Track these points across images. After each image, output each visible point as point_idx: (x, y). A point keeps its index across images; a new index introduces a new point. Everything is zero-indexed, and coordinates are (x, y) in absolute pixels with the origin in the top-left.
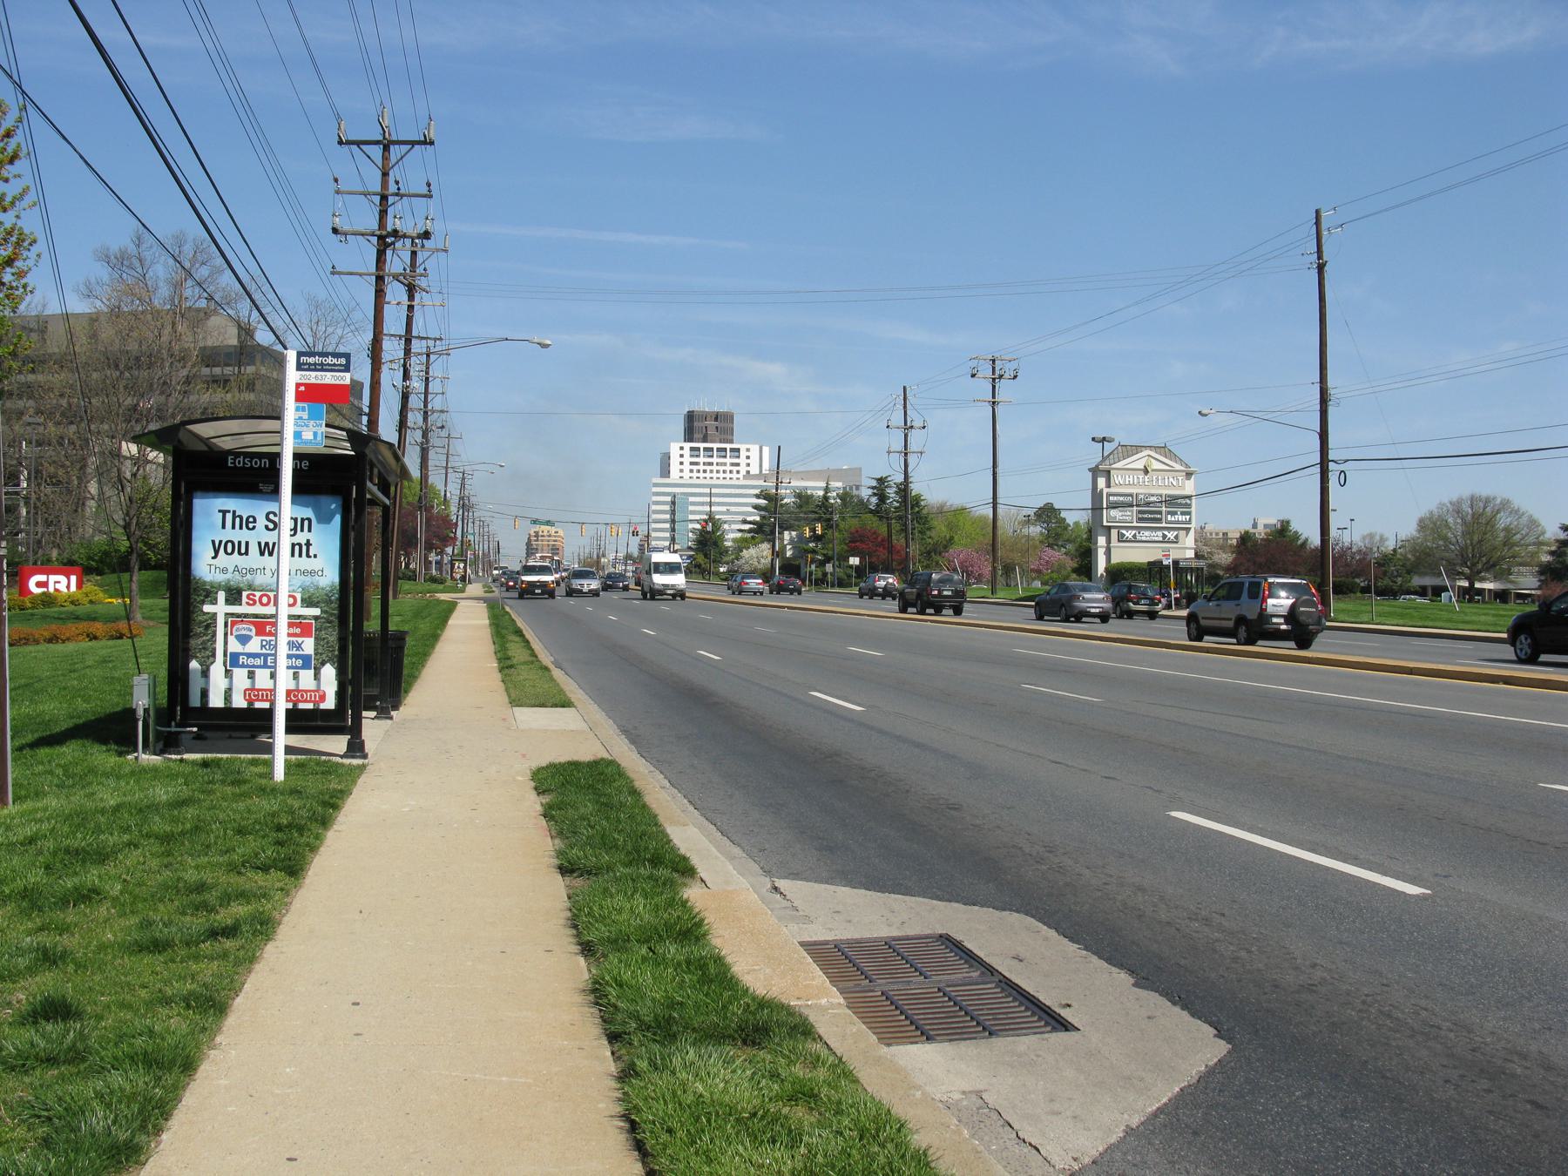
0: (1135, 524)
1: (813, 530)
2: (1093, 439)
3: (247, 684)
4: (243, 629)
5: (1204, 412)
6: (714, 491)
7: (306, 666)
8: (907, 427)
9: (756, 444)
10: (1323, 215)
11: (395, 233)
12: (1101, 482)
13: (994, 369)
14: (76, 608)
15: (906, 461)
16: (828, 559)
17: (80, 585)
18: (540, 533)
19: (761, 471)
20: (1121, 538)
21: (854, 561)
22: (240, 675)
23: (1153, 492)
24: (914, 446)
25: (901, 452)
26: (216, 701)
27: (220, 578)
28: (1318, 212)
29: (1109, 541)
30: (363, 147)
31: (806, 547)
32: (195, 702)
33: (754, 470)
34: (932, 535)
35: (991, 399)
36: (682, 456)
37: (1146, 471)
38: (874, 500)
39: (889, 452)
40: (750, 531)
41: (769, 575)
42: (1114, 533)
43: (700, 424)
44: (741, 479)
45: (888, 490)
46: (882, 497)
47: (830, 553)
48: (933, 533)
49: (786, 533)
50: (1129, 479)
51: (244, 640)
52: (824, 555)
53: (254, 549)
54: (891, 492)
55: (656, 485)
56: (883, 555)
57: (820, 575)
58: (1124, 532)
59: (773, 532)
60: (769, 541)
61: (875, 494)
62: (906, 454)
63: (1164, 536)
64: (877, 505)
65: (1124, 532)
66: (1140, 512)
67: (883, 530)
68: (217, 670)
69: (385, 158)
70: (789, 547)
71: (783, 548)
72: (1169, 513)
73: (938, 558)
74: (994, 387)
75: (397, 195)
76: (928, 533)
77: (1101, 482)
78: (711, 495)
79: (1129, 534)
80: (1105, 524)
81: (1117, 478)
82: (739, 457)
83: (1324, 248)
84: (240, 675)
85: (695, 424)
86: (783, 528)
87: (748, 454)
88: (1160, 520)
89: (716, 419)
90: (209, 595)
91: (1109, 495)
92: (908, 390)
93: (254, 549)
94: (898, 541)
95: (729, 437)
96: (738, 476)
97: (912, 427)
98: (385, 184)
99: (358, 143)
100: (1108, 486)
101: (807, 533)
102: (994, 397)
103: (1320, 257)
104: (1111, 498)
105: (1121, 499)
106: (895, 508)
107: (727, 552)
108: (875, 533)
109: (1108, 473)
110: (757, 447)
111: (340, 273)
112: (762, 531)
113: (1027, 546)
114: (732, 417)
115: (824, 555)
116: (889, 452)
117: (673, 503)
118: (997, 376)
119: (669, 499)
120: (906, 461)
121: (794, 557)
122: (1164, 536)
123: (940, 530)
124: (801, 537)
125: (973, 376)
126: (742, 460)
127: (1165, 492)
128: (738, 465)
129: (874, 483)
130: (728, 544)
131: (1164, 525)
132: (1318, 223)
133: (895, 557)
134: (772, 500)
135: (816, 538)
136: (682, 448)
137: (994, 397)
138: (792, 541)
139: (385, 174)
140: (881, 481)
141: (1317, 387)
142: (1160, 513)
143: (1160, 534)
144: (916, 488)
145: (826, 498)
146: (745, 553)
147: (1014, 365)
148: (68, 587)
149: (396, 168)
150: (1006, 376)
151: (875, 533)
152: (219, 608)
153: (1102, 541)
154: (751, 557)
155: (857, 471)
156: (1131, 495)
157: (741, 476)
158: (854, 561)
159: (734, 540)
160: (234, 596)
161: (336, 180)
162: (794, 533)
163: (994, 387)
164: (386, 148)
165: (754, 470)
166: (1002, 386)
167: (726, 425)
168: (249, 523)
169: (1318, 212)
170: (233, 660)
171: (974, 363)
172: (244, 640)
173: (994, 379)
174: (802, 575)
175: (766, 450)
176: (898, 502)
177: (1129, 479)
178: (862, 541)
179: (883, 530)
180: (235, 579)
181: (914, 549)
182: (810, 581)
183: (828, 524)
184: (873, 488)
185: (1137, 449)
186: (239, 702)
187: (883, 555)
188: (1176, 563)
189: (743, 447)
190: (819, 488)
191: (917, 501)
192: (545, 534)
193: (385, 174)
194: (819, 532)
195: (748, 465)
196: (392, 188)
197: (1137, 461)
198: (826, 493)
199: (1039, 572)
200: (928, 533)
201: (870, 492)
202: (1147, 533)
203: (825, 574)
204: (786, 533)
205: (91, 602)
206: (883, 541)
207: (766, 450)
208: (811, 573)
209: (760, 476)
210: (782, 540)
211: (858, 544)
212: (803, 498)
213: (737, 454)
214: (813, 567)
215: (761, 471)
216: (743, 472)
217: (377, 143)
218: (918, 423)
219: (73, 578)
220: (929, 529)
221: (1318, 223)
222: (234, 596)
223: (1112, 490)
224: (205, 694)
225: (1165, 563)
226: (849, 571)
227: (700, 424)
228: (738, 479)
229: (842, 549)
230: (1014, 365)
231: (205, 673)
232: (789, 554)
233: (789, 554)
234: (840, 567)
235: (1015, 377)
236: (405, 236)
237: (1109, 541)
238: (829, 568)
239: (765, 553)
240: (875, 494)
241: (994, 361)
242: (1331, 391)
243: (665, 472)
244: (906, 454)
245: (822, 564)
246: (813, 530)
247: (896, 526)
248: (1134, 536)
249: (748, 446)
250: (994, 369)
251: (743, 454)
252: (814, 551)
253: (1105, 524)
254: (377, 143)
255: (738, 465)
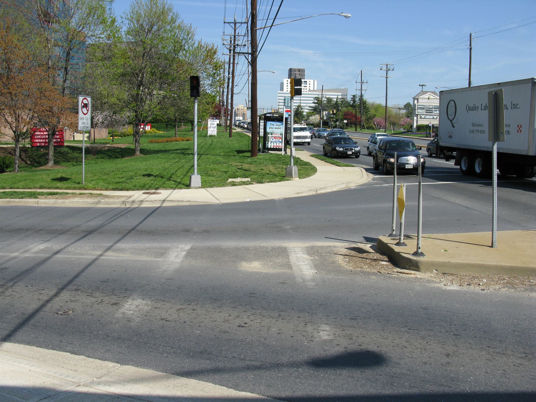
0: (425, 114)
1: (333, 111)
2: (419, 85)
3: (273, 145)
4: (273, 138)
5: (437, 87)
6: (301, 98)
7: (280, 143)
8: (362, 83)
9: (312, 79)
10: (472, 35)
11: (238, 45)
12: (416, 102)
13: (387, 68)
14: (151, 134)
15: (361, 92)
16: (337, 121)
17: (151, 128)
18: (239, 109)
19: (314, 89)
20: (421, 118)
21: (345, 121)
22: (272, 144)
23: (430, 105)
24: (364, 88)
25: (360, 90)
26: (269, 147)
27: (270, 132)
28: (471, 34)
29: (417, 118)
30: (230, 24)
31: (330, 116)
32: (267, 147)
33: (312, 89)
34: (370, 113)
35: (386, 76)
36: (287, 86)
37: (429, 99)
38: (352, 102)
39: (356, 90)
40: (312, 110)
41: (319, 125)
42: (419, 116)
43: (294, 73)
44: (307, 91)
45: (356, 99)
46: (354, 102)
47: (338, 119)
48: (370, 113)
49: (324, 112)
50: (424, 101)
51: (273, 139)
52: (336, 119)
53: (274, 128)
54: (357, 99)
55: (279, 93)
56: (354, 119)
57: (335, 125)
58: (422, 116)
59: (320, 112)
60: (318, 114)
61: (352, 100)
62: (361, 91)
63: (433, 117)
64: (353, 104)
65: (422, 116)
66: (426, 110)
67: (354, 112)
68: (269, 143)
69: (235, 27)
70: (325, 116)
71: (323, 116)
72: (435, 111)
73: (371, 121)
74: (387, 73)
75: (238, 35)
76: (368, 113)
77: (416, 102)
78: (300, 100)
79: (423, 117)
80: (416, 113)
81: (420, 101)
82: (306, 84)
83: (472, 44)
84: (272, 144)
85: (292, 73)
86: (324, 110)
87: (310, 83)
88: (432, 113)
89: (299, 71)
90: (269, 134)
91: (418, 105)
92: (362, 71)
93: (274, 128)
94: (358, 115)
95: (304, 77)
96: (306, 90)
97: (363, 82)
98: (235, 33)
99: (229, 23)
100: (418, 102)
101: (331, 112)
102: (387, 76)
103: (470, 46)
104: (418, 106)
105: (421, 106)
106: (358, 105)
107: (304, 117)
108: (352, 113)
109: (418, 99)
110: (313, 81)
111: (224, 54)
112: (316, 110)
113: (398, 116)
114: (304, 70)
115: (336, 119)
116: (356, 90)
117: (285, 100)
118: (388, 69)
119: (283, 98)
120: (361, 92)
121: (327, 119)
122: (433, 117)
123: (372, 112)
124: (329, 113)
125: (381, 69)
126: (308, 85)
127: (434, 105)
128: (306, 87)
129: (352, 97)
130: (305, 114)
131: (433, 114)
132: (470, 37)
133: (358, 120)
134: (318, 101)
135: (333, 114)
136: (287, 81)
137: (387, 76)
138: (326, 115)
139: (235, 31)
140: (354, 96)
141: (468, 81)
142: (432, 111)
143: (432, 116)
144: (365, 98)
145: (337, 101)
146: (311, 118)
147: (393, 66)
148: (148, 129)
149: (239, 29)
150: (391, 69)
151: (352, 113)
152: (270, 135)
153: (415, 118)
154: (313, 119)
155: (346, 90)
156: (424, 105)
157: (307, 90)
158: (345, 121)
159: (307, 112)
160: (272, 134)
161: (224, 33)
162: (327, 112)
163: (387, 73)
164: (235, 24)
165: (312, 89)
166: (389, 72)
167: (302, 73)
168: (273, 125)
169: (471, 34)
170: (272, 142)
171: (381, 66)
172: (273, 139)
173: (387, 71)
174: (329, 125)
175: (316, 82)
176: (359, 103)
177: (424, 101)
178: (348, 116)
179: (354, 112)
180: (272, 132)
181: (363, 118)
182: (332, 127)
183: (338, 110)
184: (352, 98)
185: (426, 92)
186: (272, 147)
187: (354, 119)
188: (433, 125)
189: (308, 81)
190: (335, 98)
191: (364, 103)
192: (241, 109)
193: (235, 31)
194: (335, 112)
195: (310, 87)
196: (237, 34)
197: (426, 96)
198: (337, 100)
199: (403, 125)
200: (368, 113)
201: (351, 99)
202: (428, 116)
203: (336, 125)
204: (324, 112)
205: (154, 132)
206: (354, 115)
207: (316, 82)
208: (332, 125)
209: (314, 91)
210: (323, 114)
211: (347, 116)
212: (329, 100)
213: (306, 83)
214: (333, 123)
215: (314, 89)
216: (308, 89)
217: (233, 23)
218: (365, 81)
219: (149, 126)
220: (369, 111)
221: (470, 37)
222: (272, 134)
223: (419, 104)
224: (268, 146)
225: (430, 125)
226: (344, 124)
227: (294, 73)
228: (306, 91)
229: (342, 118)
230: (393, 66)
231: (268, 143)
232: (325, 118)
233: (325, 118)
234: (341, 123)
235: (393, 70)
236: (240, 45)
237: (417, 118)
238: (338, 123)
239: (317, 118)
240: (352, 100)
241: (387, 65)
242: (472, 82)
243: (282, 89)
244: (361, 91)
245: (336, 122)
246: (333, 111)
247: (358, 110)
248: (425, 117)
249: (310, 80)
250: (387, 68)
251: (308, 83)
252: (333, 118)
253: (416, 113)
254: (233, 23)
255: (306, 87)
